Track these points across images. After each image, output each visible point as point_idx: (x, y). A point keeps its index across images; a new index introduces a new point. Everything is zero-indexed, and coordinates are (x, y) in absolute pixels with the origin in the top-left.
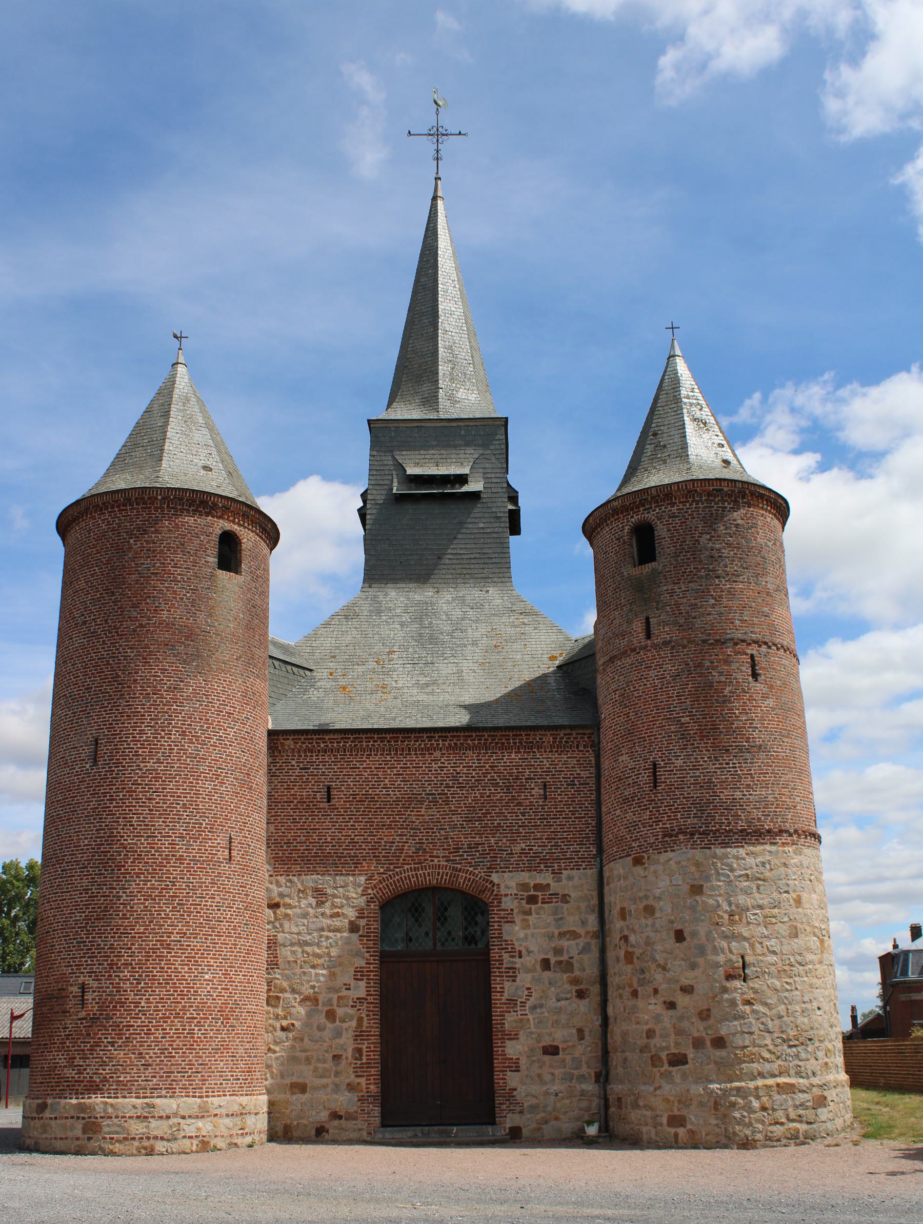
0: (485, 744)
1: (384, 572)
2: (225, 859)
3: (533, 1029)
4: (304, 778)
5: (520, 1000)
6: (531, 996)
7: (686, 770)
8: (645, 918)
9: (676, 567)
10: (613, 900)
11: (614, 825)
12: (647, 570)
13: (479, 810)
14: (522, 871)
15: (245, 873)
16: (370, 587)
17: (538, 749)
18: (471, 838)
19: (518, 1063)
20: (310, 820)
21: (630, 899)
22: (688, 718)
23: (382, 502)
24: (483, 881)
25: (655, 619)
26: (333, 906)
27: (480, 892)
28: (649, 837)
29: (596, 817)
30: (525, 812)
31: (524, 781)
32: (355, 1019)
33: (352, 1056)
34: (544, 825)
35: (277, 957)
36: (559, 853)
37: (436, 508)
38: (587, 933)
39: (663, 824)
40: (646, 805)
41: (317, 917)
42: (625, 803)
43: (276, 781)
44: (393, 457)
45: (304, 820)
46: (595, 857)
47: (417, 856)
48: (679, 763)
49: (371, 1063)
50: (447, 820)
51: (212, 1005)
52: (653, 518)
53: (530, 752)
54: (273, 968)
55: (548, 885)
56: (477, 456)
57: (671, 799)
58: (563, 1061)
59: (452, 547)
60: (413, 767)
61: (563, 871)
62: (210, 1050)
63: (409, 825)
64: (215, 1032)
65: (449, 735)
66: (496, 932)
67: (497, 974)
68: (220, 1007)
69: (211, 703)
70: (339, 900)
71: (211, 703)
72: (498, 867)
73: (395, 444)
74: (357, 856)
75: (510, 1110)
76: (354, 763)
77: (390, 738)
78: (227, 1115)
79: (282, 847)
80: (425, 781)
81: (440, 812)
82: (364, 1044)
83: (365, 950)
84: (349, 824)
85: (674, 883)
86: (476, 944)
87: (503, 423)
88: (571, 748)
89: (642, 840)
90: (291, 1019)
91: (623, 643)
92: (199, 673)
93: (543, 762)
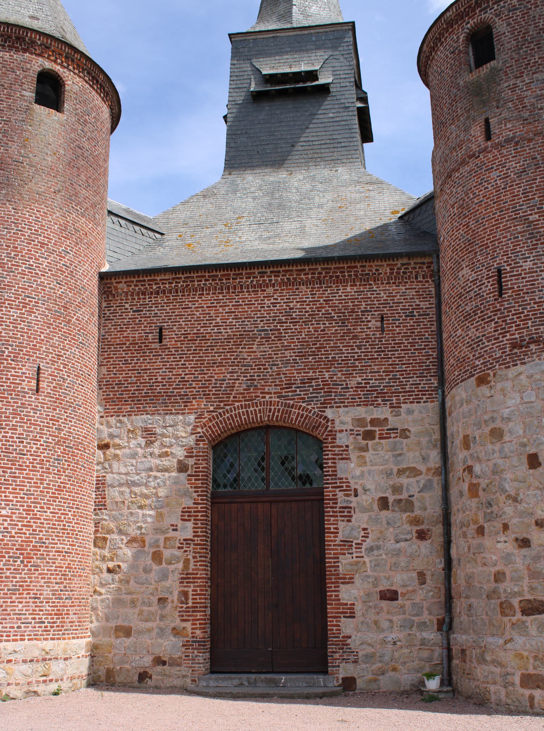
0: (319, 278)
1: (243, 161)
2: (32, 390)
3: (369, 573)
4: (137, 320)
5: (355, 541)
6: (367, 537)
7: (536, 272)
8: (492, 443)
9: (518, 60)
10: (455, 429)
11: (455, 348)
12: (485, 70)
13: (313, 345)
14: (358, 405)
15: (58, 407)
16: (230, 174)
17: (375, 281)
18: (304, 373)
19: (353, 609)
20: (141, 361)
21: (474, 425)
22: (537, 216)
23: (241, 102)
24: (317, 416)
25: (496, 119)
26: (163, 445)
27: (313, 429)
28: (495, 351)
29: (437, 348)
30: (361, 345)
31: (360, 314)
32: (182, 561)
33: (178, 599)
34: (381, 358)
35: (105, 498)
36: (397, 386)
37: (289, 105)
38: (429, 470)
39: (511, 335)
40: (490, 317)
41: (145, 457)
42: (466, 320)
43: (110, 325)
44: (251, 64)
45: (135, 361)
46: (436, 389)
47: (248, 393)
48: (528, 264)
49: (196, 607)
50: (280, 355)
51: (10, 543)
52: (491, 16)
53: (366, 285)
54: (101, 509)
55: (386, 419)
56: (326, 57)
57: (519, 306)
58: (402, 607)
59: (304, 135)
60: (245, 305)
61: (402, 405)
62: (6, 591)
63: (240, 362)
64: (12, 571)
65: (281, 270)
66: (330, 469)
67: (331, 514)
68: (19, 545)
69: (21, 231)
70: (168, 439)
71: (21, 231)
72: (333, 402)
73: (253, 53)
74: (187, 395)
75: (343, 659)
76: (187, 303)
77: (221, 275)
78: (24, 661)
79: (114, 388)
80: (257, 318)
81: (272, 347)
82: (190, 587)
83: (193, 490)
84: (180, 363)
85: (526, 400)
86: (311, 484)
87: (351, 27)
88: (409, 279)
89: (487, 356)
90: (118, 560)
91: (461, 153)
92: (9, 201)
93: (380, 294)
